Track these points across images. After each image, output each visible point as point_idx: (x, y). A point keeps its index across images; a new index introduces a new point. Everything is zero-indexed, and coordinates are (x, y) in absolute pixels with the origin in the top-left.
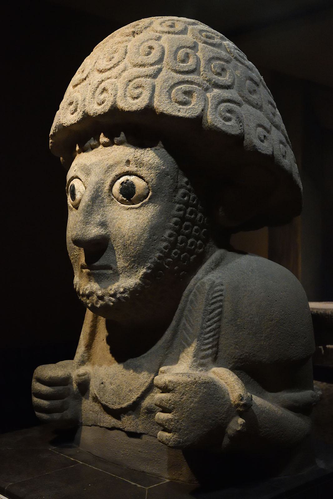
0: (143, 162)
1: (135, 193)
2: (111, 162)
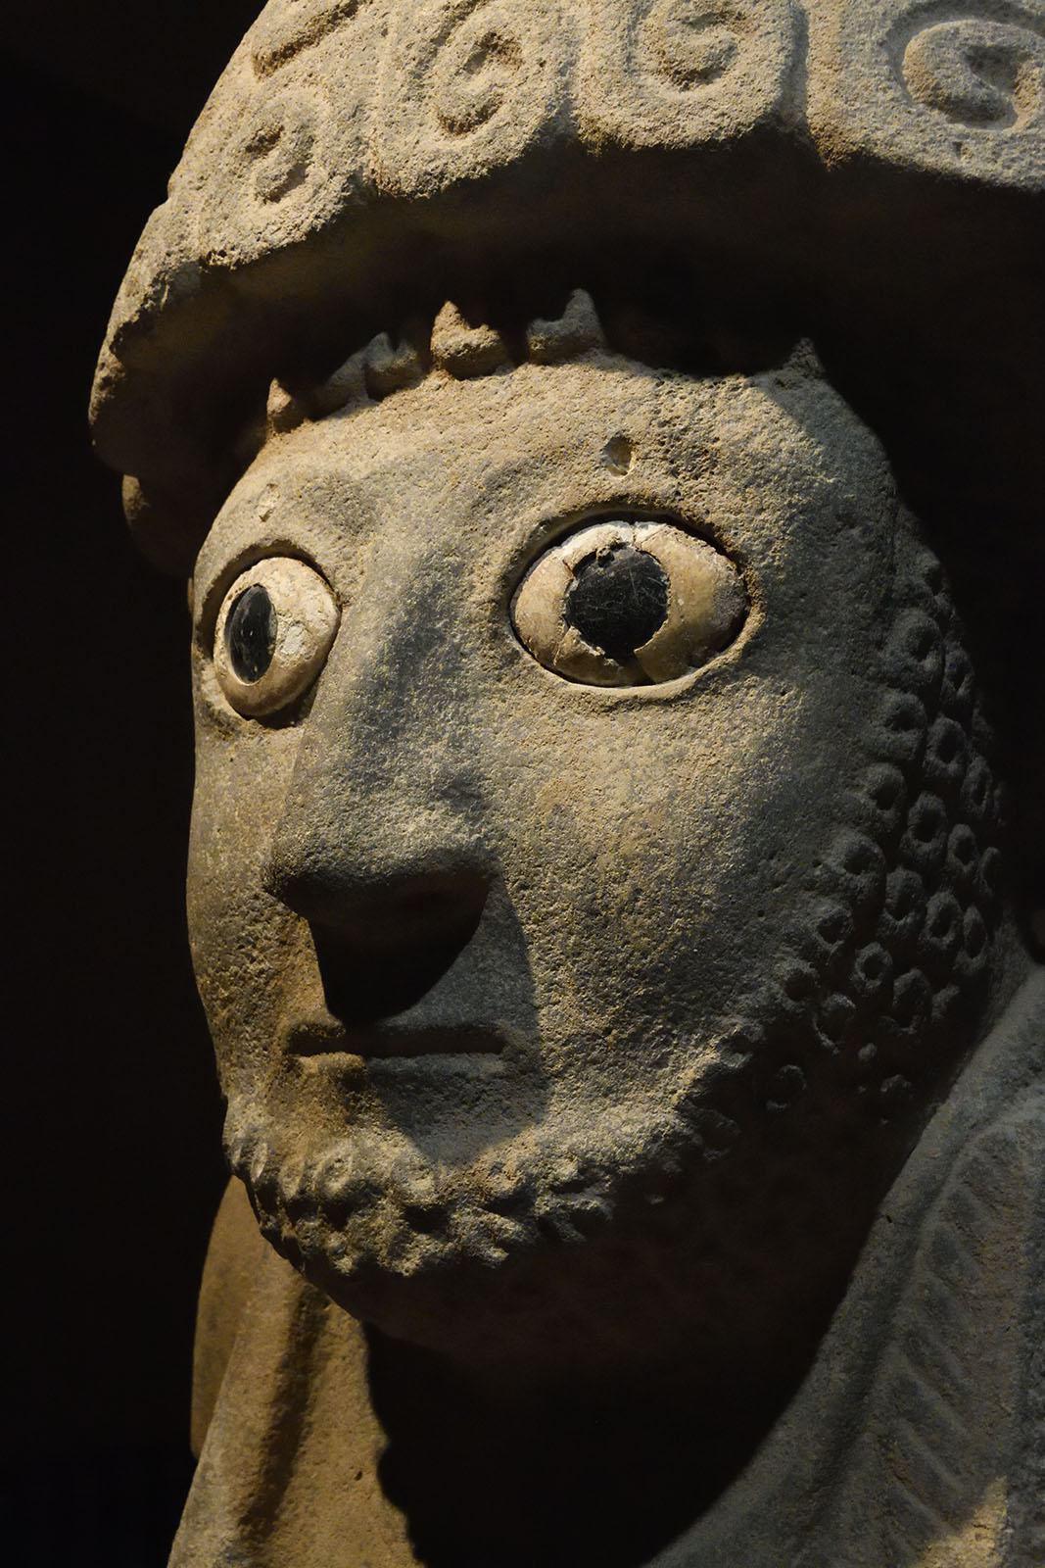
0: (709, 446)
1: (666, 617)
2: (507, 452)
